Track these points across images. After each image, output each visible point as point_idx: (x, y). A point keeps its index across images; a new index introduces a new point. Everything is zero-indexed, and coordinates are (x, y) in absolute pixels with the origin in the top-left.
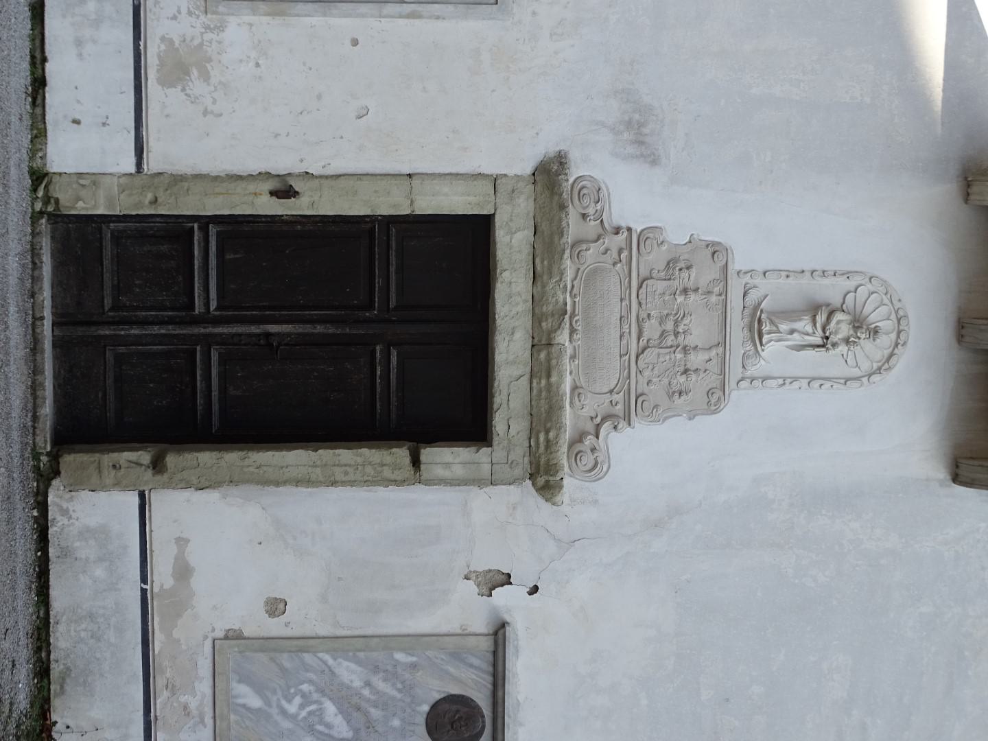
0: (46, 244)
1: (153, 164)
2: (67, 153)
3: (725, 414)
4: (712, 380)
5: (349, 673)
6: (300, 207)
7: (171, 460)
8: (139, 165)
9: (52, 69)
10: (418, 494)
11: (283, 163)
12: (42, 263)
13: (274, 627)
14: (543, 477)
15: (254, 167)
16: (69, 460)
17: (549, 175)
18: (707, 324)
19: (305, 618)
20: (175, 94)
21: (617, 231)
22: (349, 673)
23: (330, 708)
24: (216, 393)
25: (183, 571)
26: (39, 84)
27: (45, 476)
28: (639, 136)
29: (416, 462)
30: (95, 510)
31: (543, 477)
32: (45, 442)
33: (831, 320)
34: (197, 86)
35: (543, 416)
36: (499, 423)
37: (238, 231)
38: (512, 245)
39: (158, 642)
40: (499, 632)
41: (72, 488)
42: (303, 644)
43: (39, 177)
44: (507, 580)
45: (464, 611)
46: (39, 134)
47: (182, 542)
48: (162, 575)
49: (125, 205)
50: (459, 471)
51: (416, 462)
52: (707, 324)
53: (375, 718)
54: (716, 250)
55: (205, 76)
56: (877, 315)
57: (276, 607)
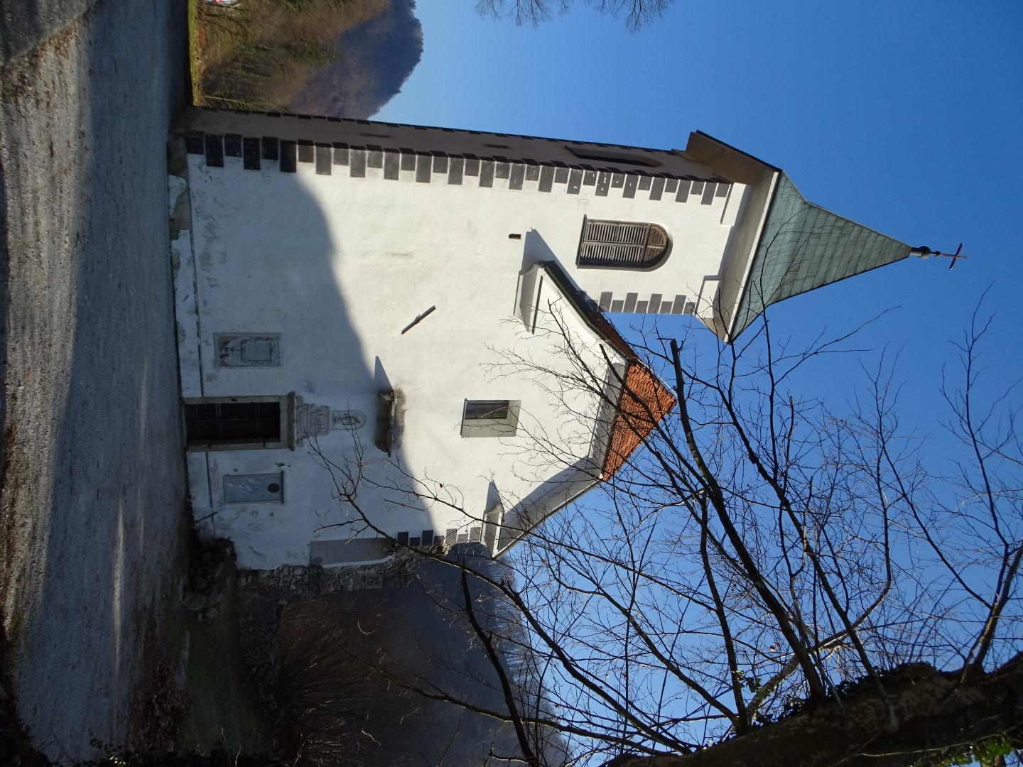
0: (183, 411)
1: (205, 395)
2: (186, 394)
3: (328, 436)
4: (326, 429)
5: (251, 481)
6: (239, 402)
7: (213, 446)
8: (202, 395)
9: (182, 379)
10: (264, 451)
11: (233, 394)
12: (600, 403)
13: (236, 473)
14: (292, 448)
15: (228, 395)
16: (190, 447)
17: (291, 396)
18: (321, 420)
19: (242, 471)
20: (209, 383)
21: (306, 405)
22: (251, 481)
23: (248, 487)
24: (284, 407)
25: (216, 465)
26: (179, 382)
27: (185, 450)
28: (310, 388)
29: (264, 445)
30: (197, 457)
31: (292, 448)
32: (185, 444)
33: (350, 419)
34: (214, 381)
35: (291, 437)
36: (281, 438)
37: (225, 407)
38: (283, 407)
39: (211, 477)
40: (282, 473)
41: (192, 452)
42: (242, 476)
43: (181, 398)
44: (283, 465)
45: (275, 469)
46: (180, 391)
47: (215, 460)
48: (211, 465)
49: (201, 403)
50: (273, 447)
51: (264, 445)
52: (321, 420)
53: (266, 444)
54: (326, 407)
55: (216, 380)
56: (361, 419)
57: (236, 470)
